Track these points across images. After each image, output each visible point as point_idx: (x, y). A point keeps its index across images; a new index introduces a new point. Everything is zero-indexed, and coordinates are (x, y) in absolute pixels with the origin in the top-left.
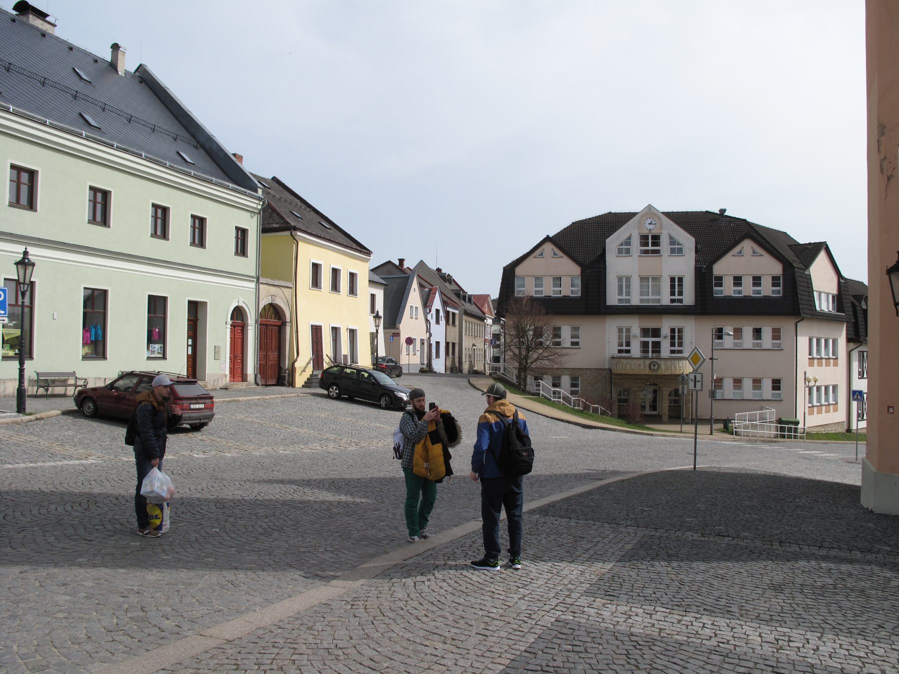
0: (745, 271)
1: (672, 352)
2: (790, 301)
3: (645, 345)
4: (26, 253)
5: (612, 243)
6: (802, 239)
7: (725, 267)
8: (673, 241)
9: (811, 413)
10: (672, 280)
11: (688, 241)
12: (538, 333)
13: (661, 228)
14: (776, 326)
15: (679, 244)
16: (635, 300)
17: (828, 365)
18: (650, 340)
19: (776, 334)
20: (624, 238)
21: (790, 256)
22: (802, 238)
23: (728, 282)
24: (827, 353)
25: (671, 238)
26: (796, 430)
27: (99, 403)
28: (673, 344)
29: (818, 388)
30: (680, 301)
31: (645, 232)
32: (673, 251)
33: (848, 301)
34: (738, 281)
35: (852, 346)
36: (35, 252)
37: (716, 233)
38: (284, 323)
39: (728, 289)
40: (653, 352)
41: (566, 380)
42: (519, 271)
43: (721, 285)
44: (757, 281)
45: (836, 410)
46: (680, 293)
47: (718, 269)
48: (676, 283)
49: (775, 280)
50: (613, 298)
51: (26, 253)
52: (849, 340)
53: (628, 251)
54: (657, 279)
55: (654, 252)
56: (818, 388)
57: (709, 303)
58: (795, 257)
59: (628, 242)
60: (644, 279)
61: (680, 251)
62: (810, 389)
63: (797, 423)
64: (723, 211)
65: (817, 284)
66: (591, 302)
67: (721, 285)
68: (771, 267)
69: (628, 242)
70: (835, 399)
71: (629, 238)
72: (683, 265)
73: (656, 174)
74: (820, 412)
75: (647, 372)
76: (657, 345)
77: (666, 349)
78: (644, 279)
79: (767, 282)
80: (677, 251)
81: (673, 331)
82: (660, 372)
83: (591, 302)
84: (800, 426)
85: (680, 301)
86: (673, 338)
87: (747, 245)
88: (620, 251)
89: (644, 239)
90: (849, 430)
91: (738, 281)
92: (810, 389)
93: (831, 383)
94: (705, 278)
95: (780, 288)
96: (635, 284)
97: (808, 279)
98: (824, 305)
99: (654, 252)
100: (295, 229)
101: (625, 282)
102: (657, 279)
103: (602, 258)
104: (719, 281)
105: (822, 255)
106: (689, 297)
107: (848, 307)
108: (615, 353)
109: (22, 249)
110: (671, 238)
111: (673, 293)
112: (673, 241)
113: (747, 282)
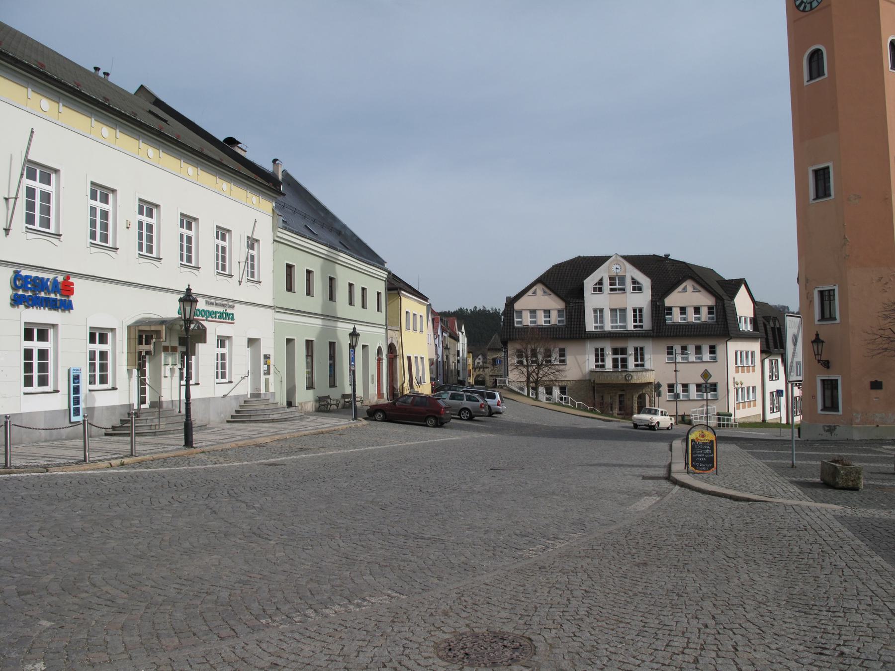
0: (687, 301)
1: (636, 366)
2: (722, 326)
3: (615, 361)
4: (354, 328)
5: (589, 283)
6: (727, 276)
7: (672, 300)
8: (634, 281)
9: (738, 408)
10: (635, 310)
11: (646, 282)
12: (548, 354)
13: (625, 271)
14: (712, 343)
15: (638, 283)
16: (608, 327)
17: (748, 371)
18: (619, 357)
19: (713, 350)
20: (597, 280)
21: (720, 291)
22: (728, 275)
23: (676, 312)
24: (747, 363)
25: (633, 279)
26: (728, 420)
27: (387, 413)
28: (636, 360)
29: (743, 389)
30: (641, 327)
31: (613, 274)
32: (634, 289)
33: (760, 322)
34: (683, 310)
35: (764, 356)
36: (359, 329)
37: (664, 273)
38: (396, 357)
39: (677, 317)
40: (622, 366)
41: (556, 392)
42: (518, 306)
43: (670, 314)
44: (697, 310)
45: (755, 405)
46: (641, 321)
47: (669, 301)
48: (638, 313)
49: (710, 309)
50: (590, 326)
51: (354, 328)
52: (762, 352)
53: (600, 290)
54: (623, 311)
55: (620, 289)
56: (743, 389)
57: (662, 329)
58: (724, 290)
59: (600, 282)
60: (613, 311)
61: (640, 289)
62: (737, 389)
63: (731, 415)
64: (667, 256)
65: (739, 312)
66: (573, 329)
67: (670, 314)
68: (705, 300)
69: (600, 282)
70: (755, 396)
71: (601, 279)
72: (643, 300)
73: (615, 225)
74: (744, 407)
75: (624, 382)
76: (624, 361)
77: (631, 363)
78: (613, 311)
79: (704, 311)
80: (638, 288)
81: (636, 349)
82: (633, 381)
83: (573, 329)
84: (733, 418)
85: (641, 327)
86: (636, 354)
87: (689, 284)
88: (595, 289)
89: (612, 280)
90: (764, 421)
91: (683, 310)
92: (737, 389)
93: (751, 385)
94: (659, 310)
95: (714, 316)
96: (607, 315)
97: (734, 307)
98: (746, 327)
99: (620, 289)
100: (401, 289)
101: (599, 312)
102: (623, 311)
103: (579, 293)
104: (669, 310)
105: (743, 287)
106: (647, 324)
107: (761, 328)
108: (593, 367)
109: (352, 326)
110: (633, 279)
111: (635, 321)
112: (634, 281)
113: (690, 312)
